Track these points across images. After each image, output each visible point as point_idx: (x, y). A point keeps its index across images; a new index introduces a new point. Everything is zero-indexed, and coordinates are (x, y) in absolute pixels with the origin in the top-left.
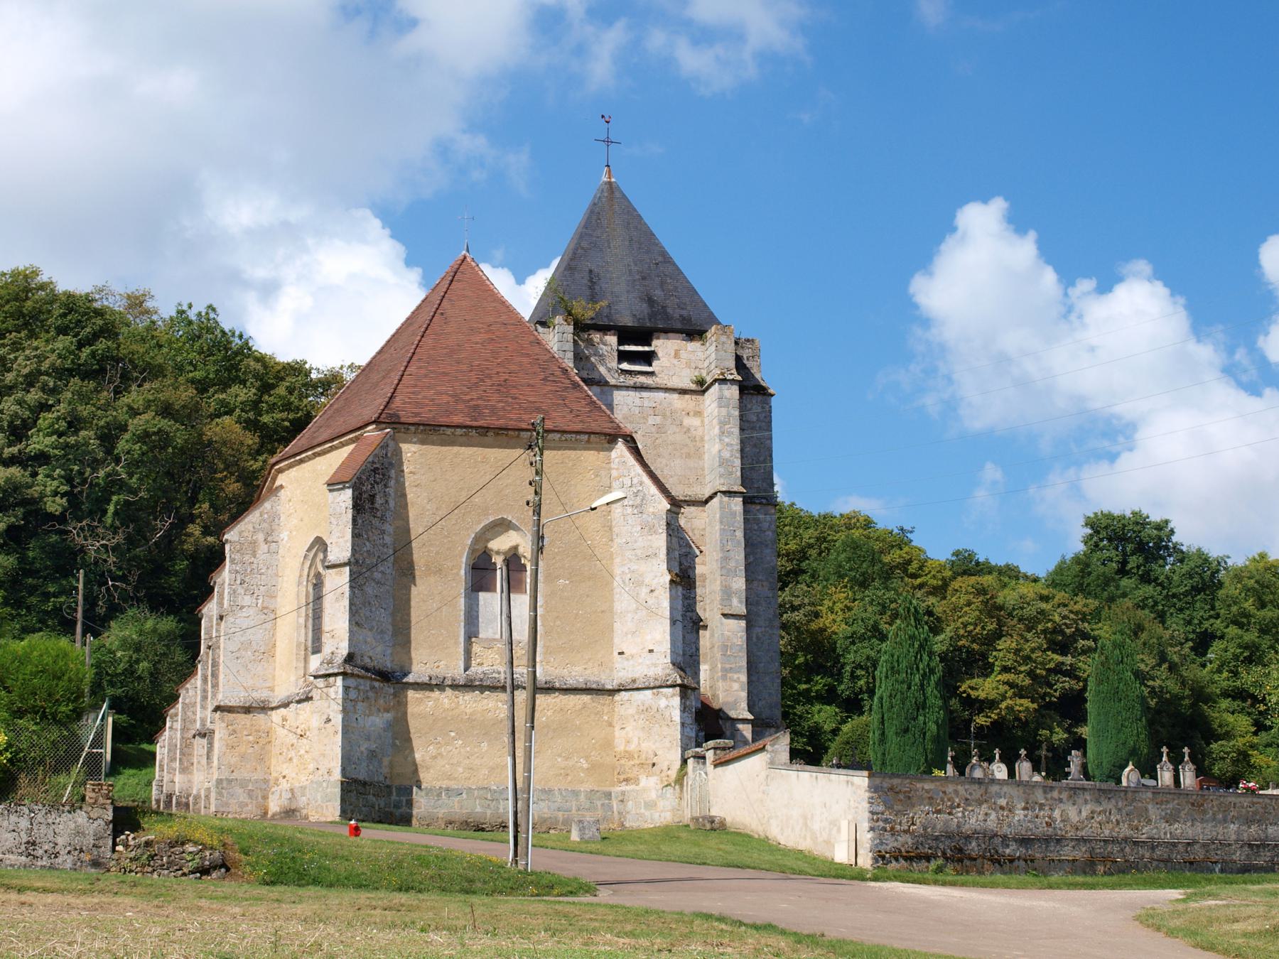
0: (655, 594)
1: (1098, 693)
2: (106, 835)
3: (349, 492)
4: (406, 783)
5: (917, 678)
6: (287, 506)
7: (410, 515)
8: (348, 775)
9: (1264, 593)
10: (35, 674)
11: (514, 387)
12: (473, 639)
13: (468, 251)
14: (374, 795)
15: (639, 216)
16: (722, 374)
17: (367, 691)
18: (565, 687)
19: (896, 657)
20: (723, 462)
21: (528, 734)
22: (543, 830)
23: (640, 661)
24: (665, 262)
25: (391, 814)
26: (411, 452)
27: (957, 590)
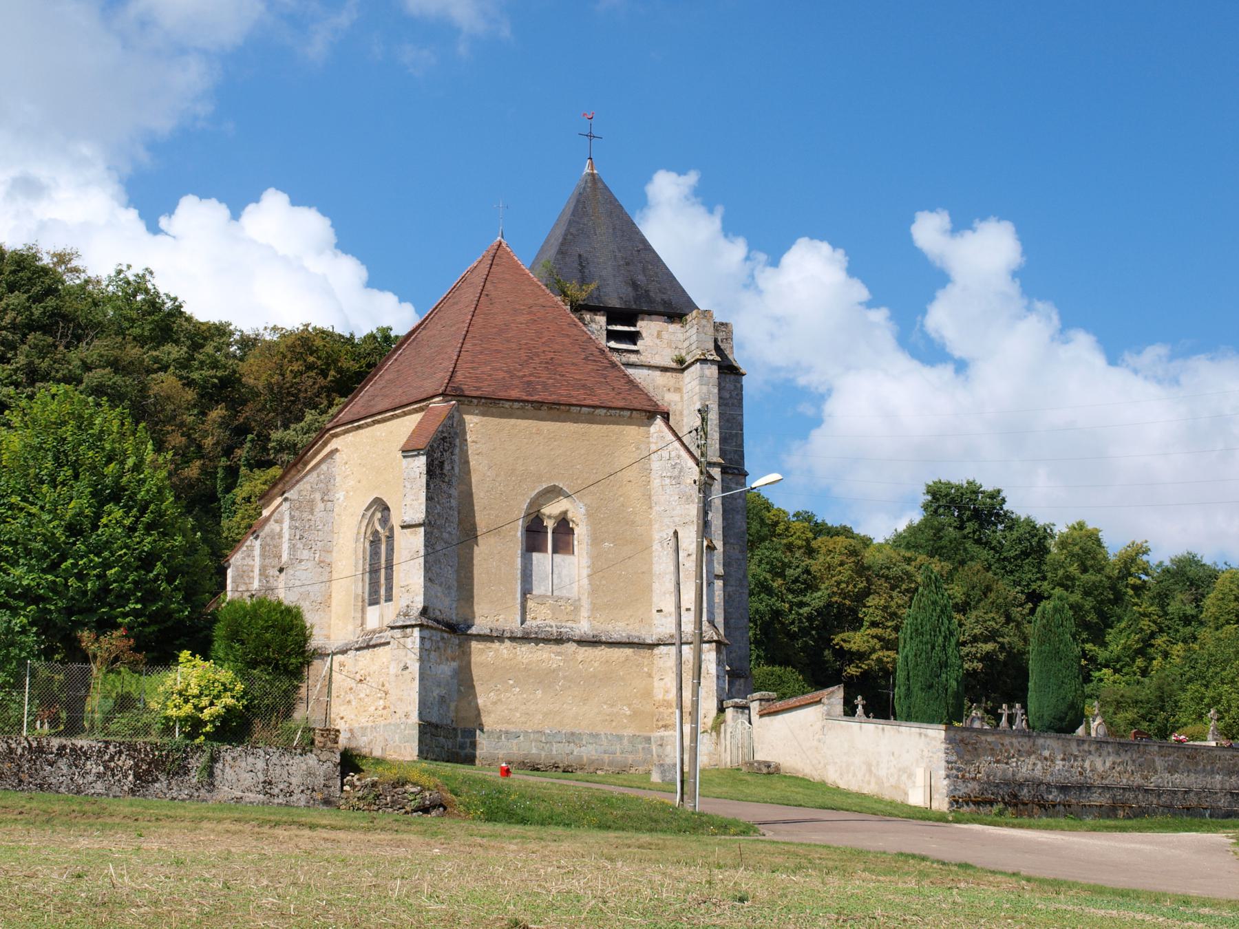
1: (1040, 653)
2: (335, 776)
3: (423, 459)
4: (470, 726)
5: (941, 640)
6: (343, 468)
7: (473, 480)
8: (423, 718)
9: (1086, 559)
10: (267, 629)
11: (561, 365)
12: (528, 596)
13: (502, 237)
14: (444, 737)
15: (621, 206)
17: (438, 642)
18: (610, 641)
19: (919, 620)
21: (695, 689)
22: (592, 770)
24: (646, 249)
25: (457, 754)
26: (472, 422)
27: (831, 551)
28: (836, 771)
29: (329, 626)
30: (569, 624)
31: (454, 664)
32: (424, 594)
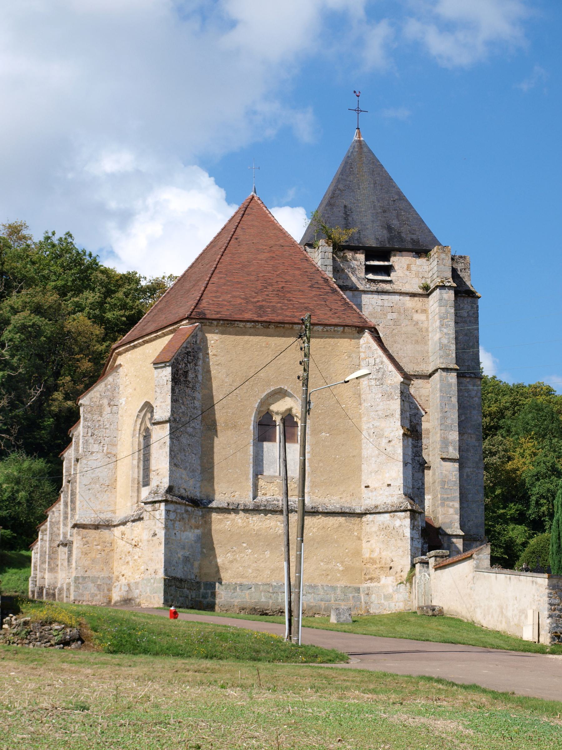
0: (392, 444)
3: (169, 370)
4: (211, 580)
6: (125, 379)
7: (214, 385)
8: (169, 574)
11: (289, 292)
12: (259, 476)
13: (255, 192)
14: (188, 589)
15: (381, 165)
16: (442, 282)
17: (182, 514)
18: (326, 511)
20: (442, 347)
21: (299, 545)
22: (311, 615)
23: (381, 492)
24: (400, 199)
25: (200, 602)
28: (481, 613)
29: (115, 503)
31: (198, 532)
32: (170, 477)
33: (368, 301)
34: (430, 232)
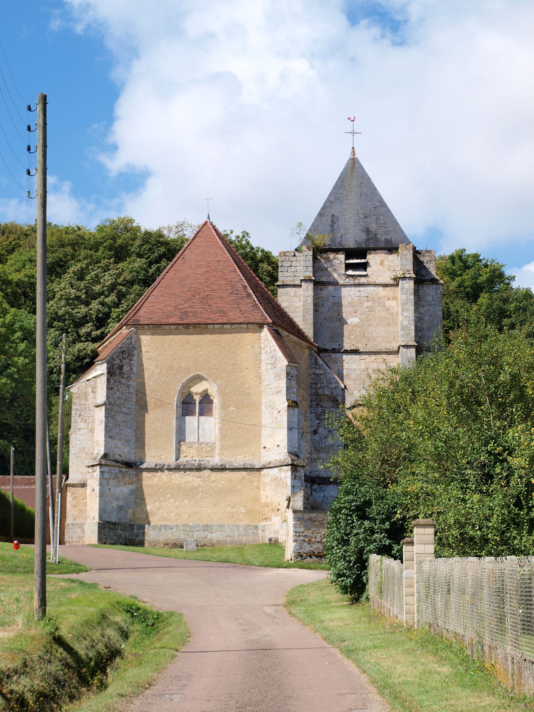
0: (280, 413)
3: (105, 365)
4: (142, 523)
8: (103, 519)
11: (212, 299)
14: (121, 530)
16: (404, 274)
17: (117, 474)
20: (403, 328)
23: (273, 451)
25: (134, 540)
30: (208, 459)
32: (105, 446)
33: (347, 293)
34: (402, 231)
